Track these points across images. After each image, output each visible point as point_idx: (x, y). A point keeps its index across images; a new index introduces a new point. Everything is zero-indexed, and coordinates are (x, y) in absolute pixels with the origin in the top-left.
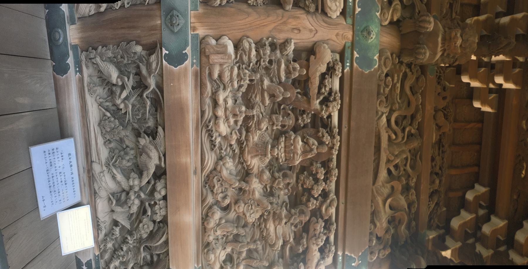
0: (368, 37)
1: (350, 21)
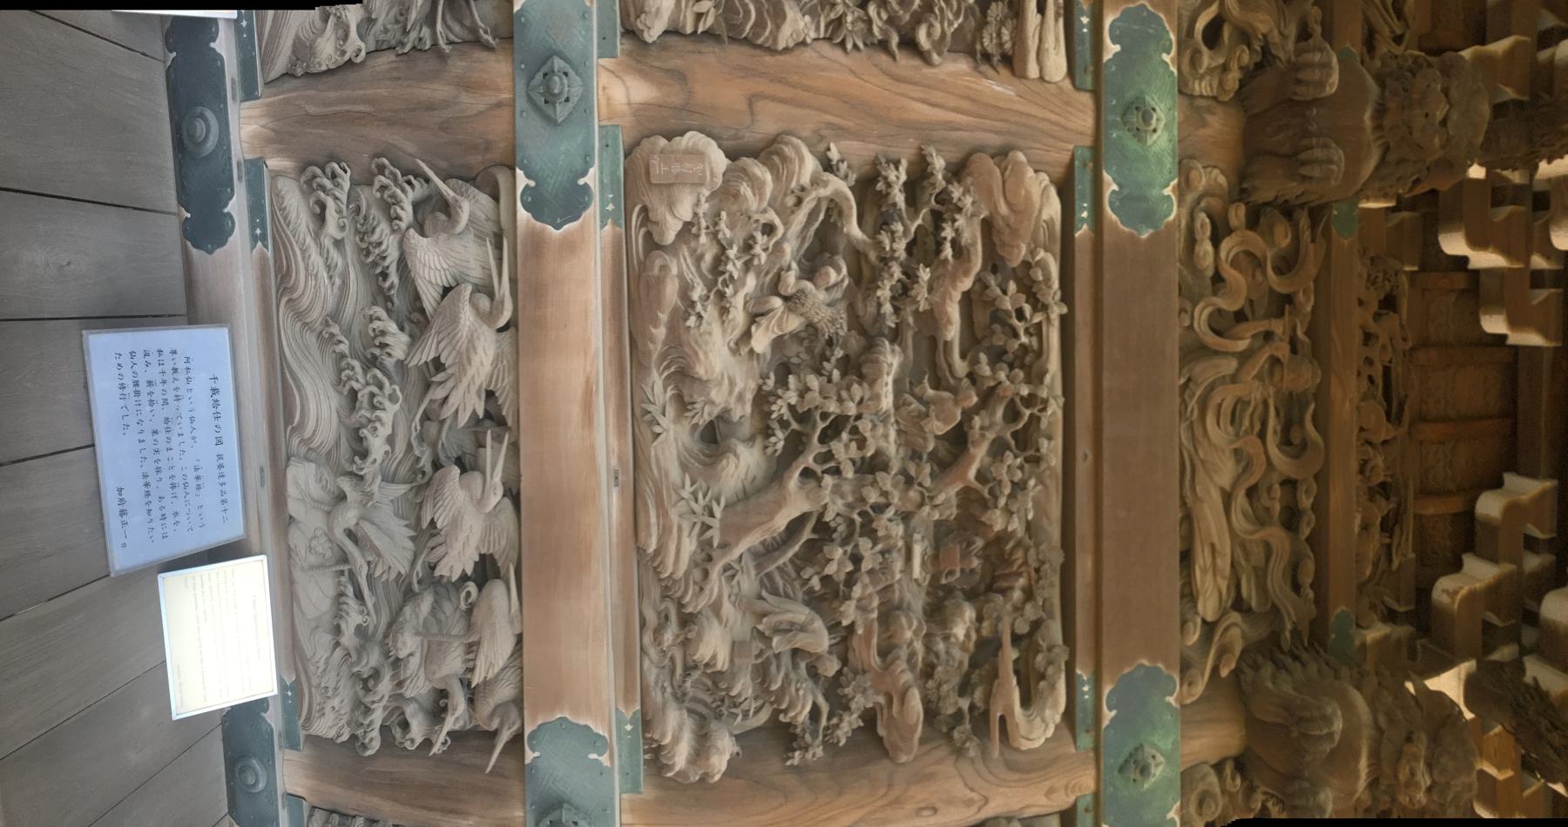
1: (1086, 740)
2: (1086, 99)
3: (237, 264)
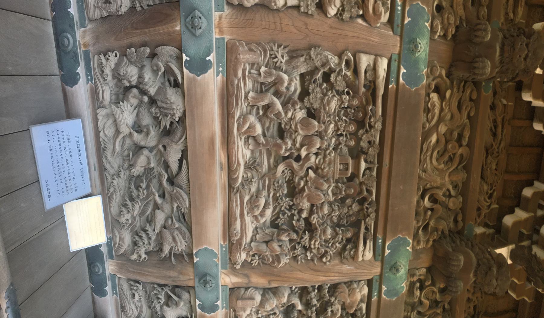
0: (415, 50)
2: (379, 264)
3: (81, 91)
